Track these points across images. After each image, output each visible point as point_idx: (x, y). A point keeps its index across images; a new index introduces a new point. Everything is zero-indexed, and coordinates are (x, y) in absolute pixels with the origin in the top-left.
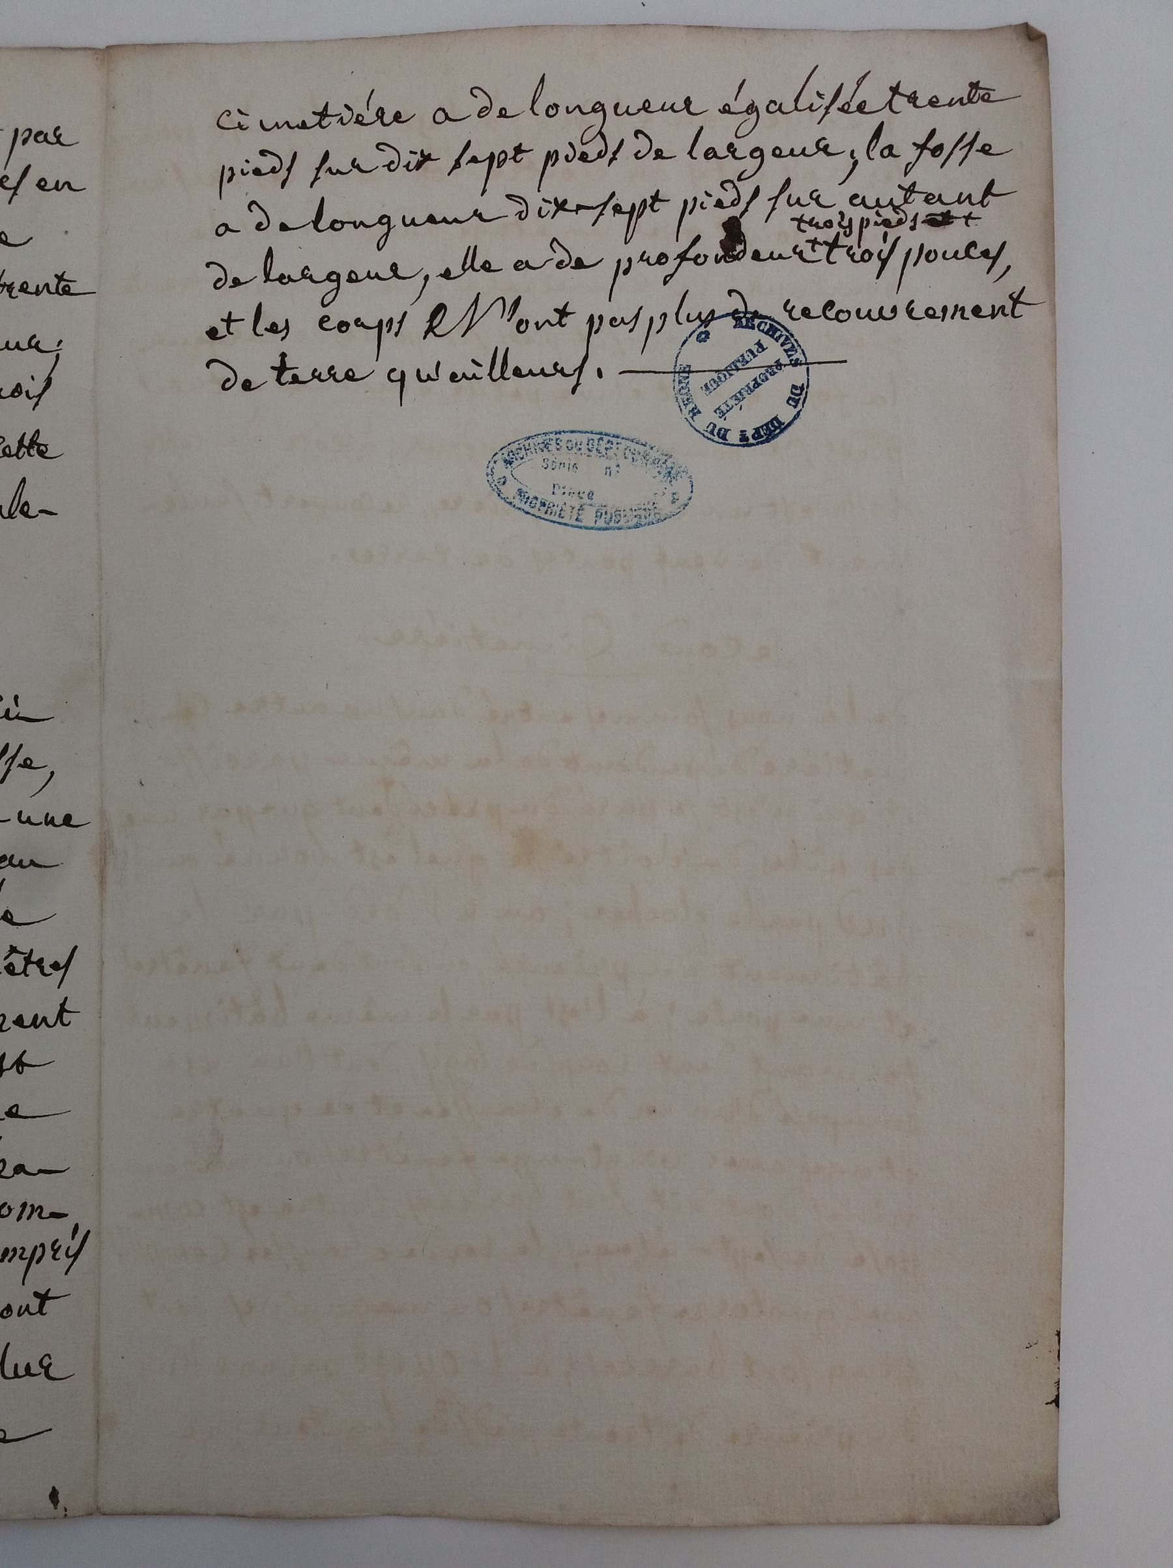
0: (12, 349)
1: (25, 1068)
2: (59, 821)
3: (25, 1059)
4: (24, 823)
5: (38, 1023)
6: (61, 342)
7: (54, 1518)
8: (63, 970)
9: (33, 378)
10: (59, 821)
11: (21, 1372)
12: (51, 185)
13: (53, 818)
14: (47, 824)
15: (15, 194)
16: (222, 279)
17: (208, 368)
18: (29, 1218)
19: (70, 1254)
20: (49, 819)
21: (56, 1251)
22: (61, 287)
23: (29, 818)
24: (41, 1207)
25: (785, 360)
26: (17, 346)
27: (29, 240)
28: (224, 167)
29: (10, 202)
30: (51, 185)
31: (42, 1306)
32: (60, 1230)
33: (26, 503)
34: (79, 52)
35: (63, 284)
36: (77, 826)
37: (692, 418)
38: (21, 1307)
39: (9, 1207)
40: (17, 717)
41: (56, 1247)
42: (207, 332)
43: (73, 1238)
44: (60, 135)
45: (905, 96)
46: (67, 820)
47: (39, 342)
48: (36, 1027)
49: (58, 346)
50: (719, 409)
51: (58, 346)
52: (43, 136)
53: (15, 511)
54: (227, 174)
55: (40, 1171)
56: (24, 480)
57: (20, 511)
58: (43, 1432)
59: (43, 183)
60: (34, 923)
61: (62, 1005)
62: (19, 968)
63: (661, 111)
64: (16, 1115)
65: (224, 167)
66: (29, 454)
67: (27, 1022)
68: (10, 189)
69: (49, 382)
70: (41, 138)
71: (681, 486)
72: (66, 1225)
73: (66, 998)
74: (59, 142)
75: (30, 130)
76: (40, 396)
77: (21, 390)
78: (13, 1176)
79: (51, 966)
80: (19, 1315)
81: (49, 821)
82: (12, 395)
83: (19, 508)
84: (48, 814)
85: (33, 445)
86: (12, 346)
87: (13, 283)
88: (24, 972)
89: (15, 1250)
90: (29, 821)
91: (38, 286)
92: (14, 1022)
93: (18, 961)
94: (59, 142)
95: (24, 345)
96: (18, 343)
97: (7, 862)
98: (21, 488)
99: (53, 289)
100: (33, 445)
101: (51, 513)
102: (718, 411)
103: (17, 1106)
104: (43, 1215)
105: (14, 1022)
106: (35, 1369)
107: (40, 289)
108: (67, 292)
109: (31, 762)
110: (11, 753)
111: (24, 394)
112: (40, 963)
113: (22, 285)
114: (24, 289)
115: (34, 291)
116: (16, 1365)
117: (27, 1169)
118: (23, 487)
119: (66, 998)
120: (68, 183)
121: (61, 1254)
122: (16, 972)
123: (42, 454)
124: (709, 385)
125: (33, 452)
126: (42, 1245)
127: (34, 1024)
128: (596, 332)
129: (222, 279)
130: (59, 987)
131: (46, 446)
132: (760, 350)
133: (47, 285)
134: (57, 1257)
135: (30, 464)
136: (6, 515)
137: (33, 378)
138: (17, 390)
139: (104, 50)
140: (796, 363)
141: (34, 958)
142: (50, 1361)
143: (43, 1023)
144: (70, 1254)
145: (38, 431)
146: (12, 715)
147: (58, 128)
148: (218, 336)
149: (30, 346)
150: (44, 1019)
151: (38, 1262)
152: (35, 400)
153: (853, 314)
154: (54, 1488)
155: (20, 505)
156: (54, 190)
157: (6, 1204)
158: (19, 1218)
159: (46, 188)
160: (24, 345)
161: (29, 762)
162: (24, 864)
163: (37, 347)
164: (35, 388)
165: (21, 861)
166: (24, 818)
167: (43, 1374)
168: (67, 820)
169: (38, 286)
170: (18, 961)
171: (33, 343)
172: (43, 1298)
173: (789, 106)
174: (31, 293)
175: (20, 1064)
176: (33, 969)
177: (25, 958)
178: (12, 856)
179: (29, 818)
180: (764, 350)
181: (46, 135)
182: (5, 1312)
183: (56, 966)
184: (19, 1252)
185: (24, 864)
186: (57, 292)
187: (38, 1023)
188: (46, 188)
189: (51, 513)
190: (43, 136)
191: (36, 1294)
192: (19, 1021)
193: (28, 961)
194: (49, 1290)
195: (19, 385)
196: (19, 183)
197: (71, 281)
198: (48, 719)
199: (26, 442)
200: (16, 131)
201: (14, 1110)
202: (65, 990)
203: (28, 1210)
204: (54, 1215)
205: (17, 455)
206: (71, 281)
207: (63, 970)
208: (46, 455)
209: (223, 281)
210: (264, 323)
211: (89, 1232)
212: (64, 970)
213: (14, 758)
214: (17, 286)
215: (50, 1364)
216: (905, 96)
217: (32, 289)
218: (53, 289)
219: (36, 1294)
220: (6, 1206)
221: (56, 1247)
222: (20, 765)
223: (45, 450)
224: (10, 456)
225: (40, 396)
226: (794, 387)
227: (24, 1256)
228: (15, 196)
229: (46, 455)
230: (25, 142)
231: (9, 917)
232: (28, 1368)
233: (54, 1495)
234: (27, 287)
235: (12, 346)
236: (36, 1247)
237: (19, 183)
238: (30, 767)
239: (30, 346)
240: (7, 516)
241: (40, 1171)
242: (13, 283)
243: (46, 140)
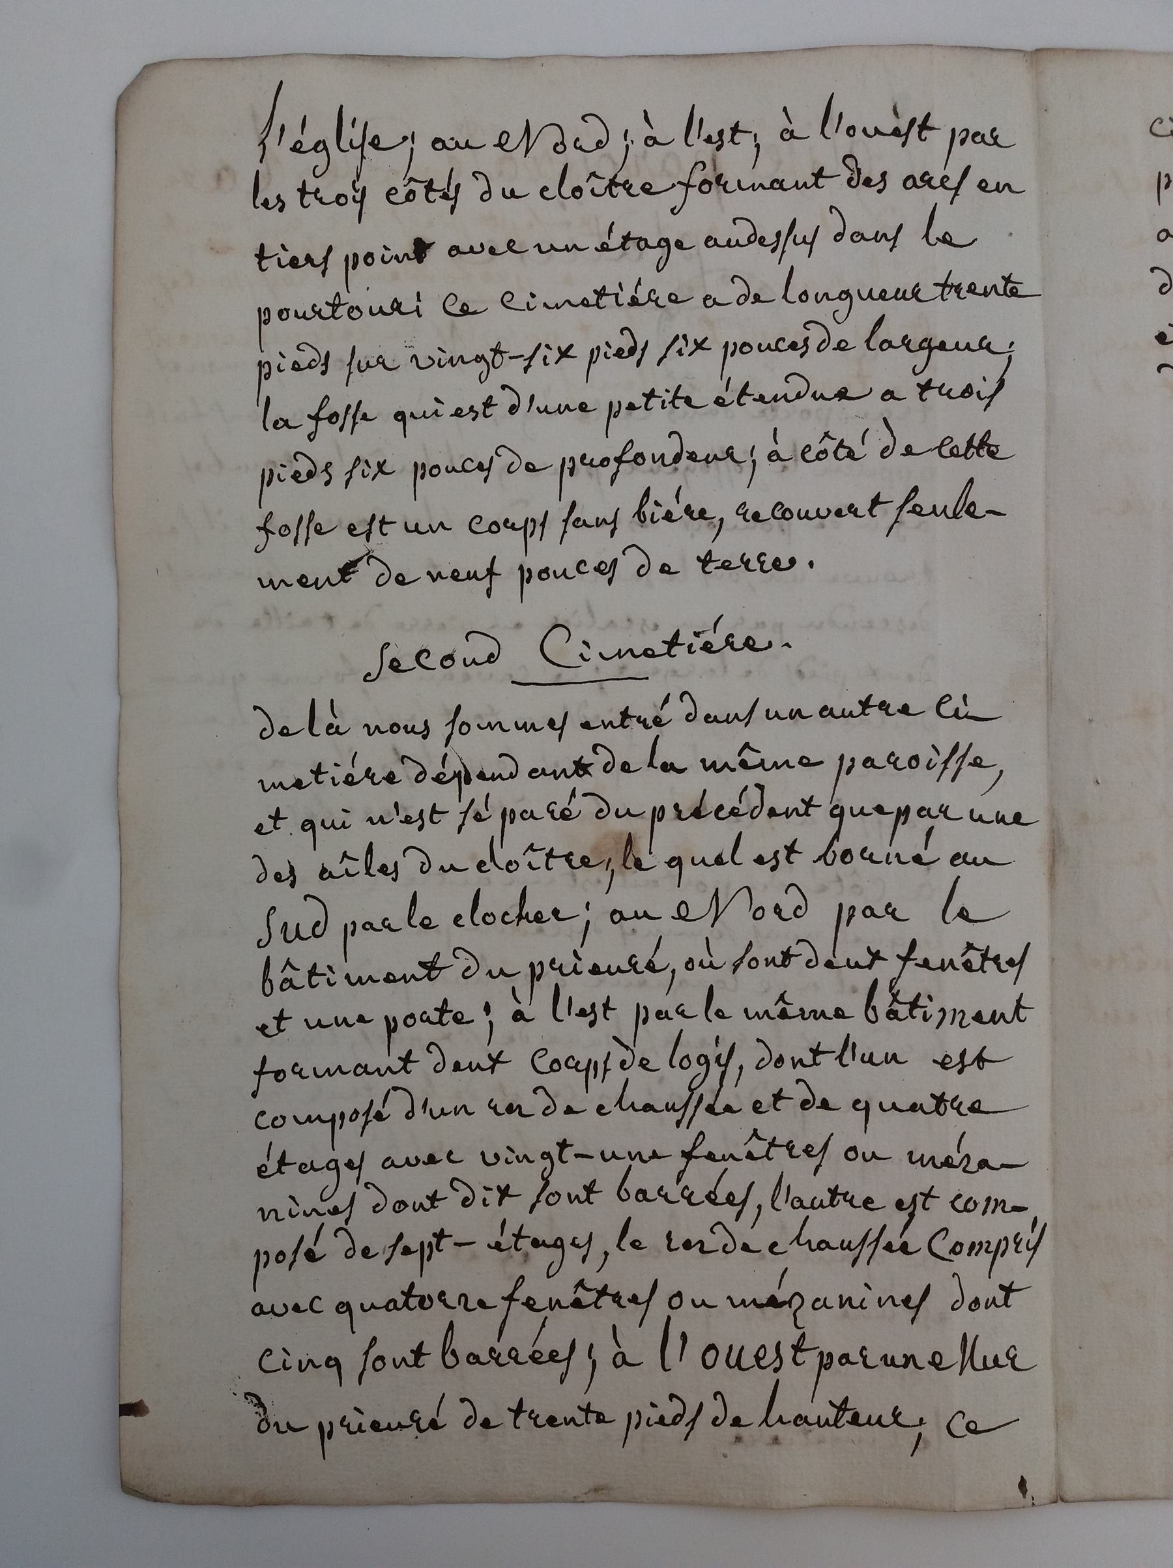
0: (962, 350)
1: (985, 1063)
2: (1009, 819)
3: (985, 1055)
4: (976, 821)
5: (996, 1019)
6: (1012, 343)
7: (1023, 1508)
8: (1018, 967)
9: (984, 379)
10: (1009, 819)
11: (990, 1363)
12: (992, 186)
13: (1003, 816)
14: (998, 822)
15: (956, 194)
16: (1167, 285)
17: (1160, 372)
18: (993, 1212)
19: (1030, 1247)
20: (1000, 817)
21: (1018, 1244)
22: (1008, 288)
23: (981, 816)
24: (1003, 1201)
26: (968, 347)
27: (973, 242)
28: (1160, 173)
29: (952, 203)
30: (992, 186)
31: (1007, 1298)
32: (1021, 1223)
33: (973, 504)
34: (1009, 54)
35: (1010, 286)
36: (1027, 824)
38: (988, 1299)
39: (975, 1202)
40: (966, 716)
41: (1018, 1240)
42: (1156, 337)
43: (1033, 1231)
44: (997, 136)
46: (1017, 818)
47: (990, 343)
48: (995, 1023)
49: (1010, 347)
51: (1010, 347)
52: (980, 137)
53: (961, 511)
54: (1164, 181)
55: (1003, 1166)
56: (971, 481)
57: (966, 512)
58: (1011, 1422)
59: (984, 184)
60: (989, 920)
61: (1018, 1001)
62: (976, 964)
64: (978, 1111)
65: (1160, 173)
66: (978, 455)
67: (986, 1018)
68: (951, 189)
69: (1001, 383)
70: (978, 139)
72: (1024, 1220)
73: (1022, 994)
74: (996, 143)
75: (967, 130)
76: (992, 397)
77: (972, 390)
78: (978, 1171)
79: (1007, 963)
80: (987, 1307)
81: (1001, 820)
82: (962, 396)
83: (965, 509)
84: (998, 812)
85: (984, 446)
86: (962, 346)
87: (961, 284)
88: (982, 968)
89: (981, 1244)
90: (980, 819)
91: (986, 287)
92: (973, 1018)
93: (975, 958)
94: (996, 143)
95: (974, 346)
96: (968, 344)
97: (961, 860)
98: (968, 488)
99: (1001, 291)
100: (984, 446)
101: (999, 514)
103: (979, 1101)
104: (1006, 1209)
105: (973, 1018)
106: (1003, 1360)
107: (988, 290)
108: (1014, 293)
109: (981, 760)
110: (961, 752)
111: (975, 395)
112: (996, 959)
113: (970, 286)
114: (972, 289)
115: (982, 292)
116: (985, 1357)
117: (990, 1164)
118: (971, 487)
119: (1022, 994)
120: (1008, 185)
121: (1022, 1247)
122: (973, 968)
123: (992, 455)
125: (983, 452)
126: (1006, 1239)
127: (993, 1020)
128: (594, 362)
129: (1167, 285)
130: (1015, 984)
131: (997, 447)
133: (994, 287)
134: (1019, 1250)
135: (980, 465)
136: (950, 515)
137: (984, 379)
138: (968, 391)
139: (1031, 52)
141: (991, 955)
142: (1015, 1353)
143: (1002, 1019)
144: (1030, 1247)
145: (989, 432)
146: (961, 714)
147: (994, 130)
148: (1167, 341)
149: (981, 348)
150: (1002, 1015)
151: (1002, 1255)
152: (987, 400)
153: (755, 347)
154: (1022, 1477)
155: (966, 506)
156: (996, 192)
157: (971, 1198)
158: (984, 1212)
159: (987, 189)
160: (974, 346)
161: (978, 761)
162: (978, 862)
163: (988, 348)
164: (987, 389)
165: (975, 859)
166: (976, 817)
167: (1010, 1364)
168: (1017, 818)
169: (986, 287)
170: (975, 958)
171: (984, 344)
172: (1008, 1290)
174: (980, 295)
175: (980, 1060)
176: (989, 965)
177: (982, 955)
178: (966, 854)
179: (981, 816)
181: (983, 136)
182: (973, 1305)
183: (1011, 963)
184: (985, 1245)
185: (978, 862)
186: (1005, 293)
187: (996, 1019)
188: (987, 189)
189: (999, 514)
190: (980, 137)
191: (1002, 1287)
192: (978, 1017)
193: (985, 957)
194: (1013, 1282)
195: (969, 386)
196: (960, 183)
197: (1018, 283)
198: (996, 718)
199: (976, 443)
200: (953, 130)
201: (976, 1106)
202: (1021, 987)
203: (992, 1204)
204: (1016, 1209)
205: (965, 455)
206: (1018, 283)
207: (1018, 967)
208: (997, 456)
209: (1168, 287)
211: (1046, 1224)
212: (1018, 966)
213: (964, 756)
214: (965, 287)
215: (1016, 1355)
217: (980, 290)
218: (1001, 291)
219: (1002, 1287)
220: (972, 1202)
221: (1018, 1240)
222: (970, 764)
223: (995, 451)
224: (957, 456)
225: (992, 397)
227: (989, 1250)
228: (957, 197)
229: (997, 456)
230: (963, 142)
231: (965, 913)
232: (996, 1359)
233: (1022, 1484)
234: (975, 288)
235: (962, 346)
236: (1000, 1240)
237: (960, 183)
238: (980, 766)
239: (981, 348)
240: (952, 516)
241: (1003, 1166)
242: (961, 284)
243: (983, 140)
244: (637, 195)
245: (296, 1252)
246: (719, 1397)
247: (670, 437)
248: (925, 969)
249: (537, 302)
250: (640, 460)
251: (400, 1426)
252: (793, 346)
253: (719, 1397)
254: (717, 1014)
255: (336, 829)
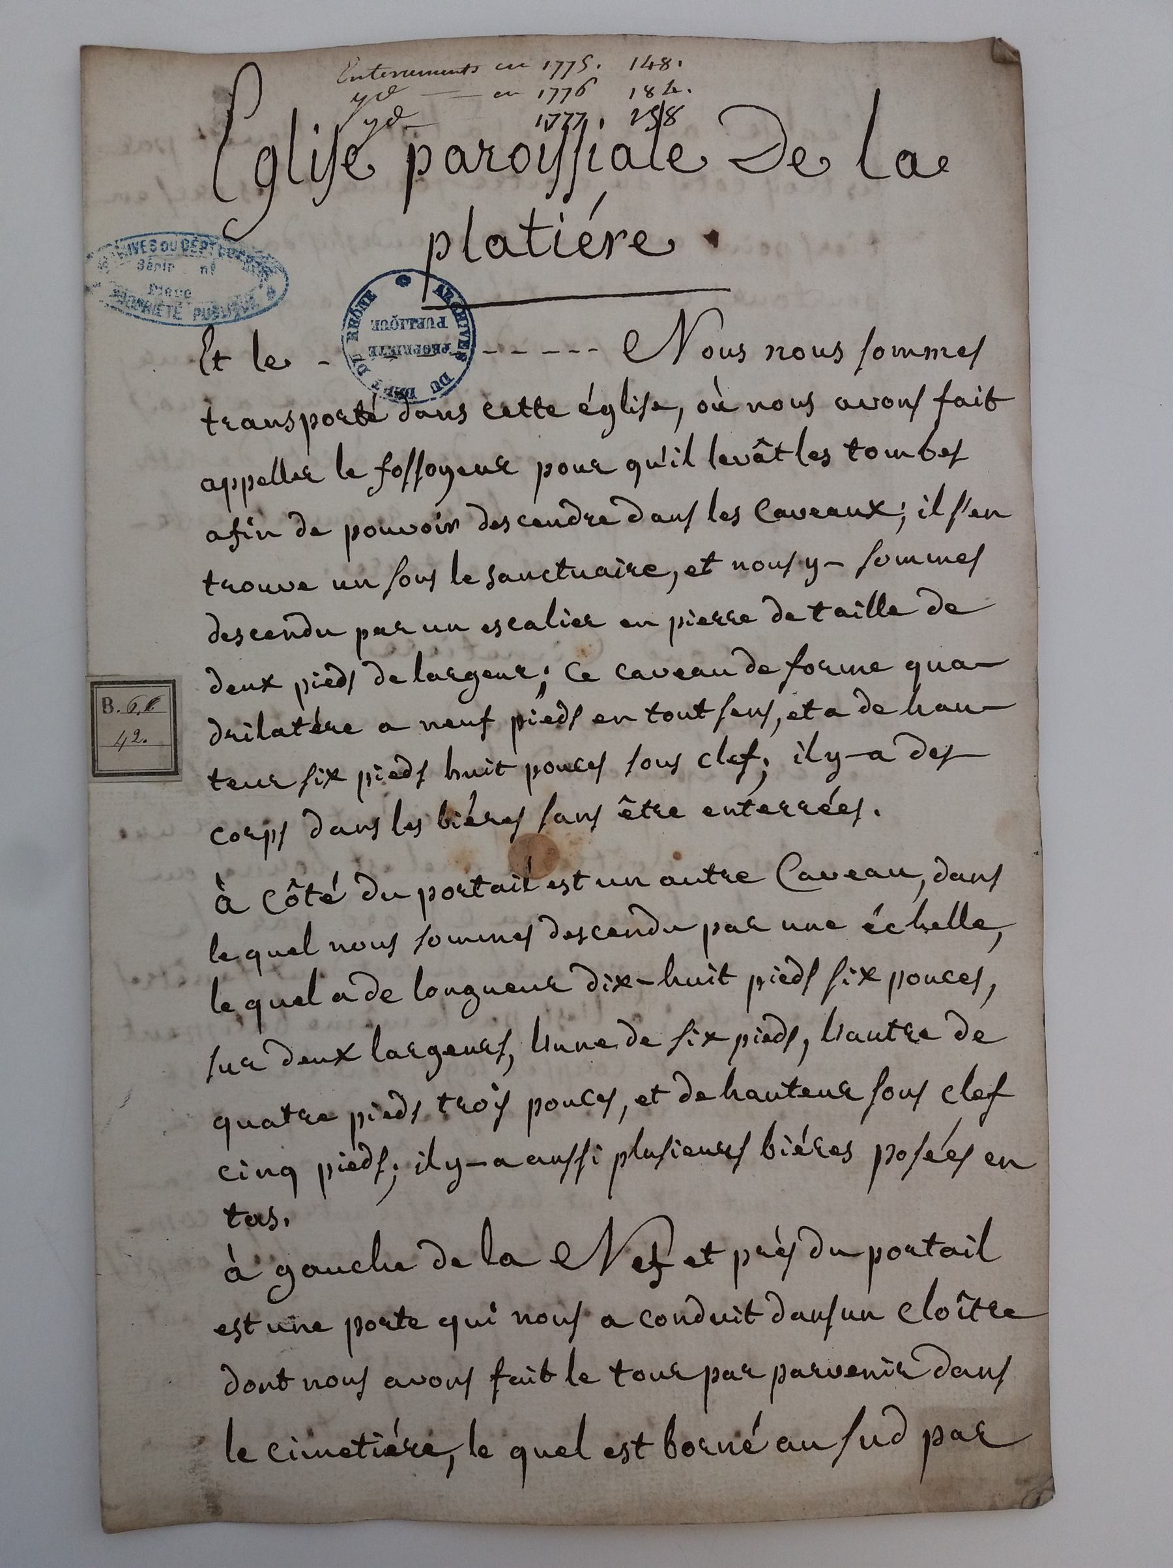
25: (454, 348)
37: (348, 339)
45: (463, 1053)
50: (374, 347)
63: (463, 994)
71: (277, 281)
102: (372, 349)
124: (380, 323)
132: (441, 325)
140: (460, 356)
173: (541, 623)
180: (444, 326)
210: (218, 953)
216: (463, 1053)
226: (445, 375)
244: (920, 563)
245: (917, 1153)
246: (858, 693)
247: (763, 601)
248: (806, 1098)
249: (250, 1172)
250: (799, 354)
251: (471, 724)
252: (963, 979)
253: (858, 693)
254: (581, 1378)
255: (771, 1101)
